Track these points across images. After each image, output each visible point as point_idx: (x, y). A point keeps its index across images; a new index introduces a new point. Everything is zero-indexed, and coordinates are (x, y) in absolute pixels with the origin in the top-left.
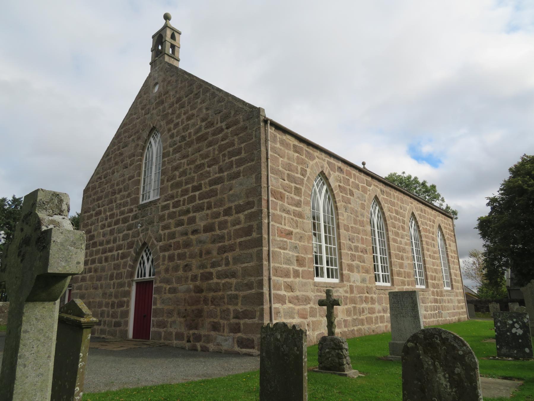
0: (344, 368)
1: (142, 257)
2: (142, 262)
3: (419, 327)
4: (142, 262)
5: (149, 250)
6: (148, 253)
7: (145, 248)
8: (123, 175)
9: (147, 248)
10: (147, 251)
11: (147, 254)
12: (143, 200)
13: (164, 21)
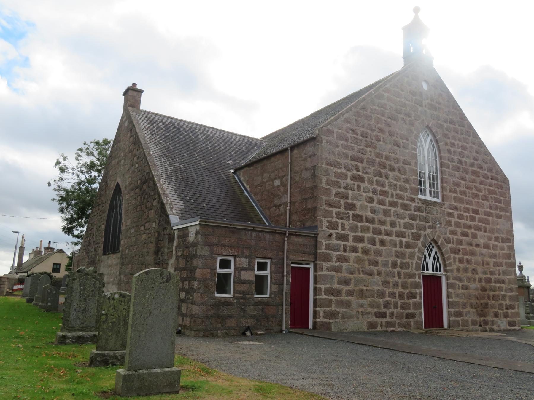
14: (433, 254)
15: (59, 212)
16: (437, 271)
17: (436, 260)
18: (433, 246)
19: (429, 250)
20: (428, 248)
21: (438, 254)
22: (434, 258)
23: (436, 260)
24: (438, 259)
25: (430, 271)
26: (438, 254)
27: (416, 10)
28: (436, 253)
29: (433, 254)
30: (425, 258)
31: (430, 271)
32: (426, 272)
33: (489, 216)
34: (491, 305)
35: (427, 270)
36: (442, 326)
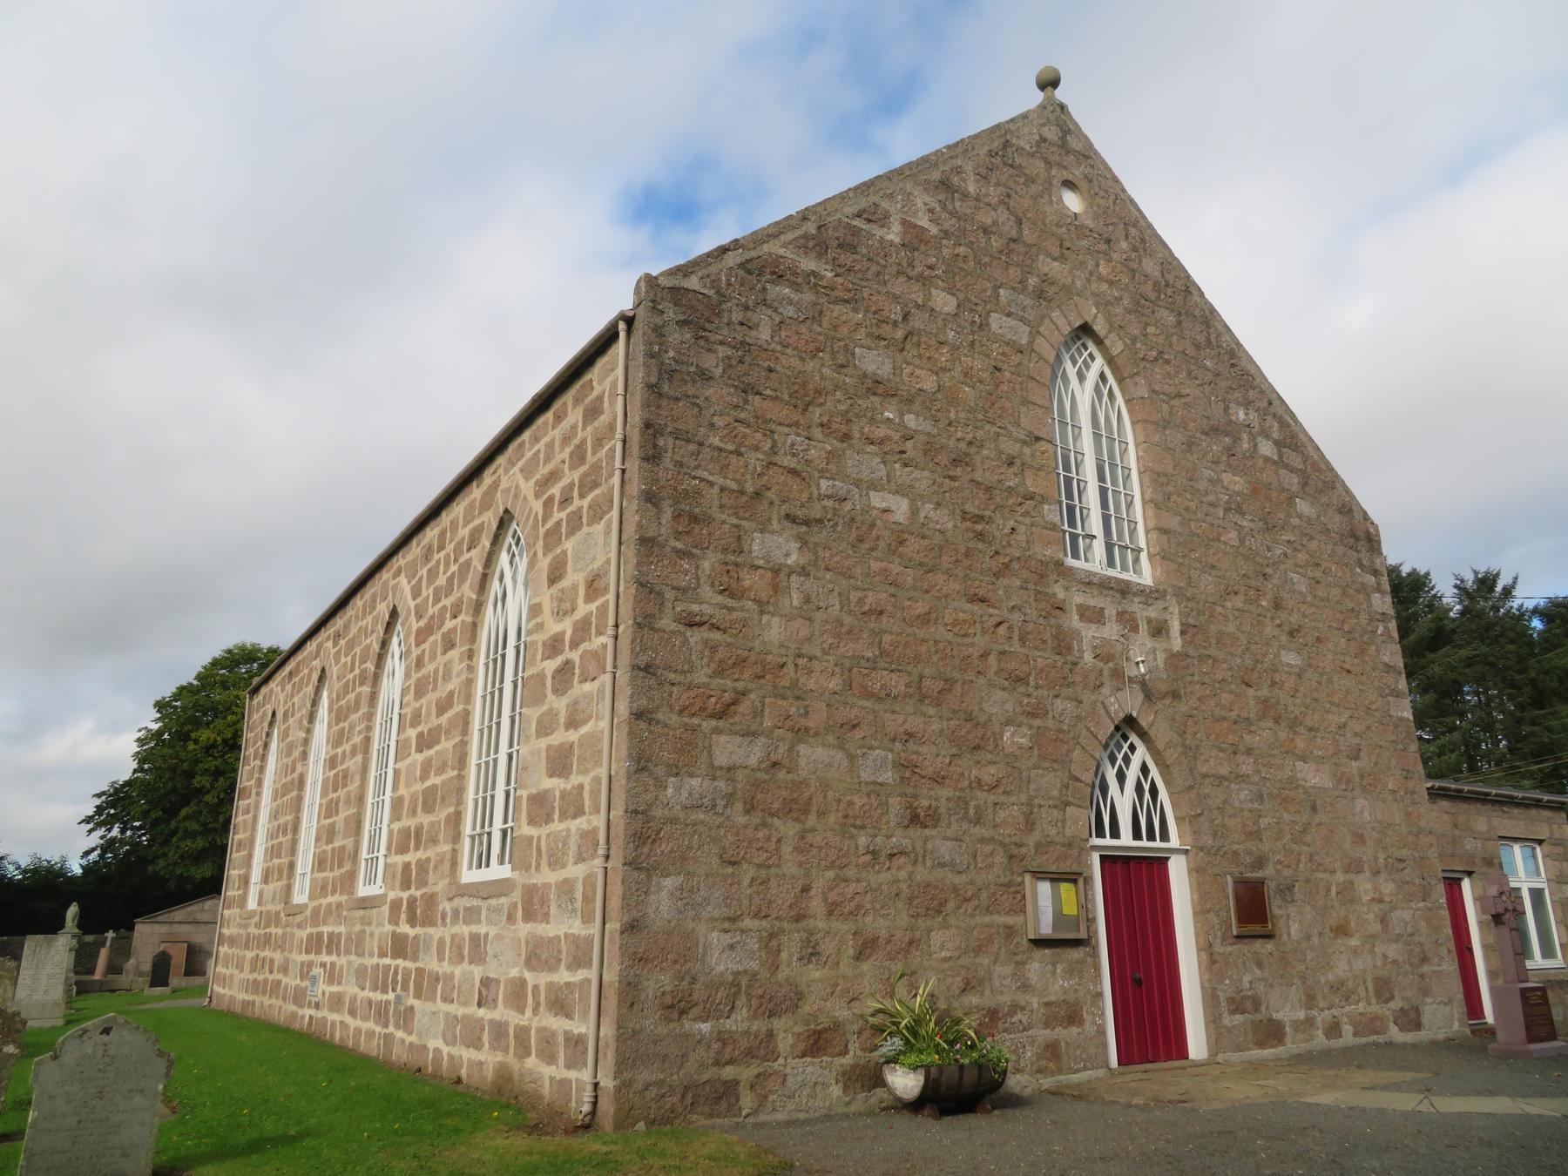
2: (1147, 787)
4: (1147, 787)
14: (1133, 773)
15: (1428, 574)
16: (1104, 837)
17: (1147, 796)
18: (1132, 744)
19: (1119, 761)
20: (1126, 753)
21: (1154, 772)
22: (1139, 789)
23: (1147, 796)
24: (1154, 791)
25: (1126, 838)
26: (1154, 772)
27: (1049, 82)
28: (1144, 769)
29: (1133, 773)
30: (1104, 789)
31: (1126, 838)
32: (1108, 841)
33: (416, 694)
34: (574, 911)
35: (1115, 833)
36: (1182, 1053)
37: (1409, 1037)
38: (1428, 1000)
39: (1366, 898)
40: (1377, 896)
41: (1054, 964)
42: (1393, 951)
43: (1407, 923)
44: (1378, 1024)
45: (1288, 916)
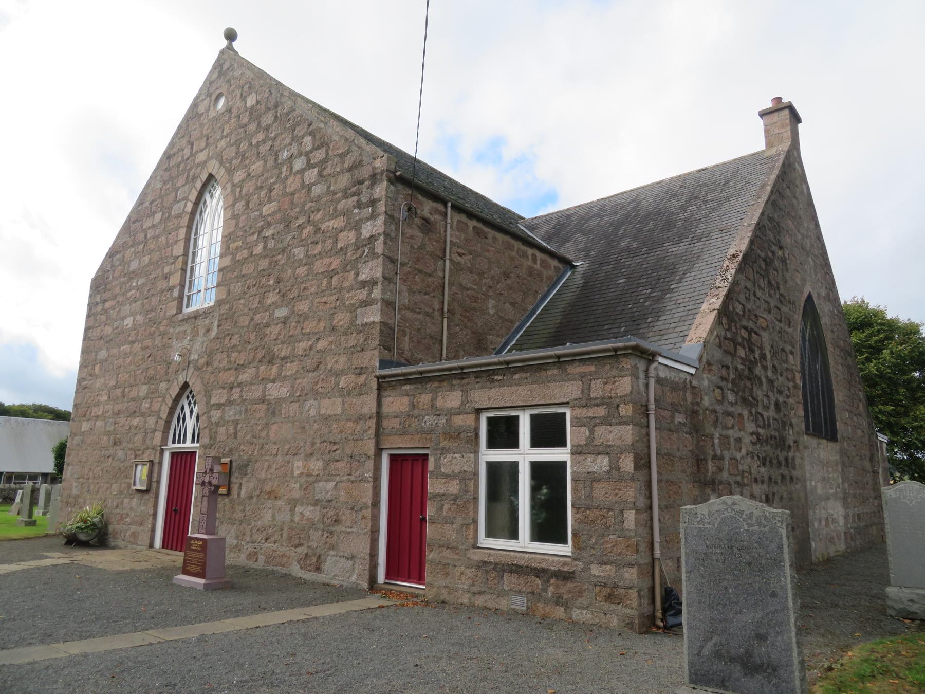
0: (708, 499)
1: (183, 408)
2: (182, 417)
3: (663, 485)
4: (182, 417)
5: (193, 397)
6: (192, 402)
7: (187, 392)
8: (336, 502)
9: (191, 392)
10: (190, 398)
11: (190, 404)
12: (187, 307)
13: (224, 43)
27: (231, 36)
37: (309, 576)
38: (332, 553)
39: (297, 473)
40: (305, 471)
41: (141, 500)
42: (309, 512)
43: (327, 492)
44: (285, 559)
45: (241, 484)
